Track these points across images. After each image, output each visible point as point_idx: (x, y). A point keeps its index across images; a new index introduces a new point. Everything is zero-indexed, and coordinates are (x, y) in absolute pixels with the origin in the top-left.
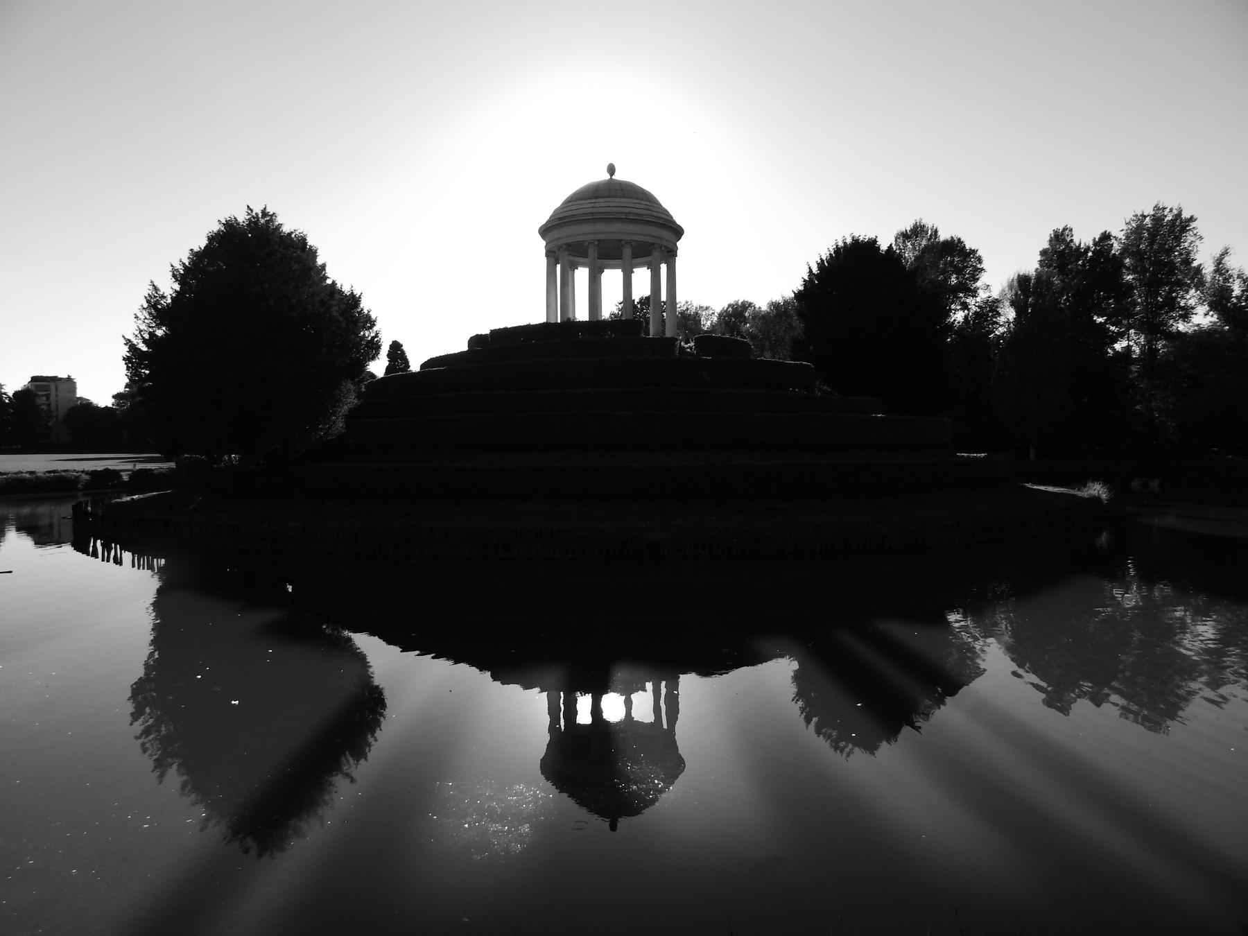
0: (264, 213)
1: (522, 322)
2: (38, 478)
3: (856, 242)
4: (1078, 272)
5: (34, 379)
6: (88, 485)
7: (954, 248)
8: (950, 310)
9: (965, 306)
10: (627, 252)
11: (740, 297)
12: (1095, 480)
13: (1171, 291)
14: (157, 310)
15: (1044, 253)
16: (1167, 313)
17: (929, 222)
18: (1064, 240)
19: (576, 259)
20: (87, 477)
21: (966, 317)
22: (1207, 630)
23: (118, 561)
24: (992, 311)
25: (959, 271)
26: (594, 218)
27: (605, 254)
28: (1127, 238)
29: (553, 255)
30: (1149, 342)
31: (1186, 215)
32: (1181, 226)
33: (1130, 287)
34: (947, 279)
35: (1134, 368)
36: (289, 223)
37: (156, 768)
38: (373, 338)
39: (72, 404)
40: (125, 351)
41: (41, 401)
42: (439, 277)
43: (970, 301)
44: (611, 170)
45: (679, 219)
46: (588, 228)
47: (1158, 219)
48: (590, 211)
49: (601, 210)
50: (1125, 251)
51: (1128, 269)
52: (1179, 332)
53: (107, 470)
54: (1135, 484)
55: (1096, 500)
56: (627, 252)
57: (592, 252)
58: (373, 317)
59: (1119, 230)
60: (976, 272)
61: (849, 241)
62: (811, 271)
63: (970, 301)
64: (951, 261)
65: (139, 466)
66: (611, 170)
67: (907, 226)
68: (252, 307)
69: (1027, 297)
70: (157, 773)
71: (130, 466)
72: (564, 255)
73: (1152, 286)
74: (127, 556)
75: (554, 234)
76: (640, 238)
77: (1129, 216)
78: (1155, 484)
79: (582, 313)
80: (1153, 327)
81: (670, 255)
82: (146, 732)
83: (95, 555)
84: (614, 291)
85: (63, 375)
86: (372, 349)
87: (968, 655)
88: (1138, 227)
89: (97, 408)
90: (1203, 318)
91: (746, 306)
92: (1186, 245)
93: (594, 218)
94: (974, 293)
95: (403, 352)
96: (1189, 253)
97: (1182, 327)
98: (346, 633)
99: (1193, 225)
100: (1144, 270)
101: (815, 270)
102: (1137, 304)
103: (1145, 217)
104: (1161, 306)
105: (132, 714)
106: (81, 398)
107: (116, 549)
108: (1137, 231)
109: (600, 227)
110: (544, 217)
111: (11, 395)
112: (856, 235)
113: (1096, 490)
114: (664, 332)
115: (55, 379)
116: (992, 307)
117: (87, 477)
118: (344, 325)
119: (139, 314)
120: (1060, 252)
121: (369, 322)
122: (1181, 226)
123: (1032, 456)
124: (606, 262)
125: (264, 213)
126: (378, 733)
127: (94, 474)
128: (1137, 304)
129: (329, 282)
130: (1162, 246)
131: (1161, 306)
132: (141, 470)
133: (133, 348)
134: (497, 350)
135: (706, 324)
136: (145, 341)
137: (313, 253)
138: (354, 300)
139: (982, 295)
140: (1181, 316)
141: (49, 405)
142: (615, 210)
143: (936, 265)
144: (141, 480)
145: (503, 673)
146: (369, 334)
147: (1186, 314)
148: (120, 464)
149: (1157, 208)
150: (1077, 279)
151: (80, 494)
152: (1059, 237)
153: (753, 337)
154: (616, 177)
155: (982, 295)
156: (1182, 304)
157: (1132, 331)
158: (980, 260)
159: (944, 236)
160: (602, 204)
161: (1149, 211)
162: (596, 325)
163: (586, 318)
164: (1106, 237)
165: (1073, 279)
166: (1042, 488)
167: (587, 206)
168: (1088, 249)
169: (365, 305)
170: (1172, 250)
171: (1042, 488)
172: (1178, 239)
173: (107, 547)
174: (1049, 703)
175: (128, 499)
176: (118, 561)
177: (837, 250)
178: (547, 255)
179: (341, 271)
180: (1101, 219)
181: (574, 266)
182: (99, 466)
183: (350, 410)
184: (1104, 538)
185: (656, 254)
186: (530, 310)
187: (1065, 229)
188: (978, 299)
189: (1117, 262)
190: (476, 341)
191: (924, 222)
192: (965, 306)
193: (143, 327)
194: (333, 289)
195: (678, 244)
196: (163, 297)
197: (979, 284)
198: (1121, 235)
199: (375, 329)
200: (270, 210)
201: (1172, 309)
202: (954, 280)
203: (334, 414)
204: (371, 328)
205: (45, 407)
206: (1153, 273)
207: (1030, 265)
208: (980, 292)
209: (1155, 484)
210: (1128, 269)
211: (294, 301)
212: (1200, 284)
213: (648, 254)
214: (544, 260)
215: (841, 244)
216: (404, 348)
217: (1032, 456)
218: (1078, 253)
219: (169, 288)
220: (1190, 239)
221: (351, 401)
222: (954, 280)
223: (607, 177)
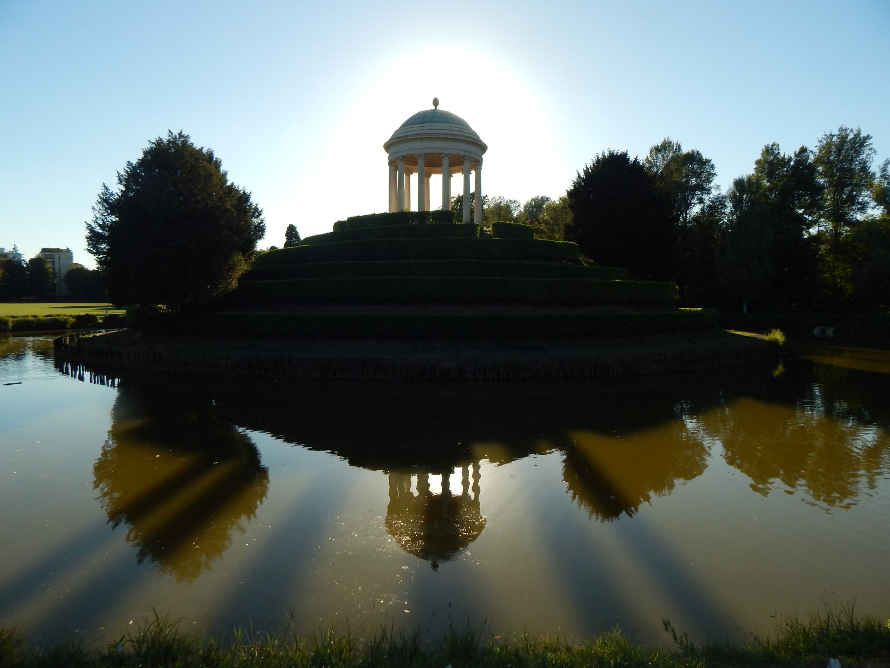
0: (180, 135)
1: (369, 212)
2: (39, 320)
3: (612, 155)
4: (784, 176)
5: (44, 250)
6: (74, 326)
7: (693, 158)
8: (691, 203)
9: (701, 201)
10: (445, 162)
11: (540, 194)
12: (776, 328)
13: (852, 191)
14: (109, 204)
15: (758, 162)
16: (849, 206)
17: (674, 140)
18: (773, 153)
19: (412, 167)
20: (74, 320)
21: (702, 210)
22: (869, 436)
23: (81, 378)
24: (721, 204)
25: (698, 175)
26: (422, 138)
27: (431, 163)
28: (820, 151)
29: (392, 163)
30: (835, 228)
31: (863, 134)
32: (859, 143)
33: (822, 188)
34: (688, 181)
35: (823, 247)
36: (199, 141)
37: (110, 520)
38: (259, 224)
39: (70, 268)
40: (87, 233)
41: (48, 265)
42: (308, 180)
43: (706, 197)
44: (436, 102)
45: (484, 139)
46: (418, 144)
47: (843, 139)
48: (418, 132)
49: (427, 132)
50: (819, 160)
51: (820, 174)
52: (857, 221)
53: (87, 315)
54: (816, 331)
55: (775, 343)
56: (445, 162)
57: (421, 161)
58: (260, 209)
59: (814, 147)
60: (711, 176)
61: (607, 154)
62: (579, 176)
63: (706, 197)
64: (690, 168)
65: (110, 312)
66: (436, 102)
67: (659, 143)
68: (175, 204)
69: (742, 194)
70: (111, 523)
71: (103, 312)
72: (401, 164)
73: (838, 186)
74: (87, 375)
75: (394, 149)
76: (455, 152)
77: (821, 136)
78: (830, 331)
79: (414, 208)
80: (838, 217)
81: (477, 164)
82: (105, 495)
83: (67, 373)
84: (437, 193)
85: (64, 248)
86: (258, 231)
87: (699, 450)
88: (828, 143)
89: (87, 271)
90: (875, 212)
91: (544, 200)
92: (864, 156)
93: (422, 138)
94: (708, 191)
95: (297, 233)
96: (865, 162)
97: (859, 217)
98: (240, 430)
99: (869, 142)
100: (833, 175)
101: (582, 174)
102: (826, 200)
103: (833, 136)
104: (845, 202)
105: (95, 482)
106: (307, 240)
107: (80, 369)
108: (827, 148)
109: (426, 144)
110: (387, 137)
111: (27, 261)
112: (612, 150)
113: (777, 336)
114: (472, 220)
115: (58, 250)
116: (719, 203)
117: (74, 320)
118: (235, 215)
119: (96, 207)
120: (770, 162)
121: (257, 212)
122: (859, 143)
123: (745, 310)
124: (433, 169)
125: (180, 135)
126: (264, 499)
127: (78, 317)
128: (826, 200)
129: (229, 184)
130: (846, 157)
131: (845, 202)
132: (111, 315)
133: (92, 230)
134: (353, 231)
135: (515, 214)
136: (99, 225)
137: (217, 164)
138: (245, 197)
139: (714, 193)
140: (859, 209)
141: (54, 269)
142: (437, 131)
143: (678, 170)
144: (110, 321)
145: (358, 459)
146: (256, 221)
147: (863, 207)
148: (97, 310)
149: (841, 130)
150: (785, 183)
151: (68, 331)
152: (769, 151)
153: (546, 222)
154: (439, 108)
155: (714, 193)
156: (860, 200)
157: (822, 220)
158: (713, 167)
159: (685, 150)
160: (428, 128)
161: (836, 132)
162: (423, 215)
163: (417, 210)
164: (803, 150)
165: (779, 181)
166: (740, 333)
167: (416, 129)
168: (790, 159)
169: (254, 200)
170: (852, 161)
171: (740, 333)
172: (858, 153)
173: (74, 369)
174: (754, 488)
175: (91, 336)
176: (81, 378)
177: (598, 161)
178: (390, 164)
179: (238, 174)
180: (801, 135)
181: (409, 173)
182: (82, 312)
183: (243, 274)
184: (779, 370)
185: (467, 163)
186: (375, 201)
187: (773, 145)
188: (711, 196)
189: (812, 169)
190: (339, 225)
191: (670, 139)
192: (701, 201)
193: (98, 216)
194: (231, 190)
195: (483, 156)
196: (112, 194)
197: (712, 185)
198: (816, 150)
199: (261, 217)
200: (185, 133)
201: (853, 203)
202: (693, 181)
203: (230, 277)
204: (258, 216)
205: (51, 270)
206: (839, 178)
207: (748, 170)
208: (713, 190)
209: (830, 331)
210: (820, 174)
211: (199, 198)
212: (869, 186)
213: (461, 163)
214: (387, 168)
215: (600, 156)
216: (298, 230)
217: (745, 310)
218: (784, 162)
219: (117, 189)
220: (867, 152)
221: (243, 267)
222: (693, 181)
223: (433, 108)
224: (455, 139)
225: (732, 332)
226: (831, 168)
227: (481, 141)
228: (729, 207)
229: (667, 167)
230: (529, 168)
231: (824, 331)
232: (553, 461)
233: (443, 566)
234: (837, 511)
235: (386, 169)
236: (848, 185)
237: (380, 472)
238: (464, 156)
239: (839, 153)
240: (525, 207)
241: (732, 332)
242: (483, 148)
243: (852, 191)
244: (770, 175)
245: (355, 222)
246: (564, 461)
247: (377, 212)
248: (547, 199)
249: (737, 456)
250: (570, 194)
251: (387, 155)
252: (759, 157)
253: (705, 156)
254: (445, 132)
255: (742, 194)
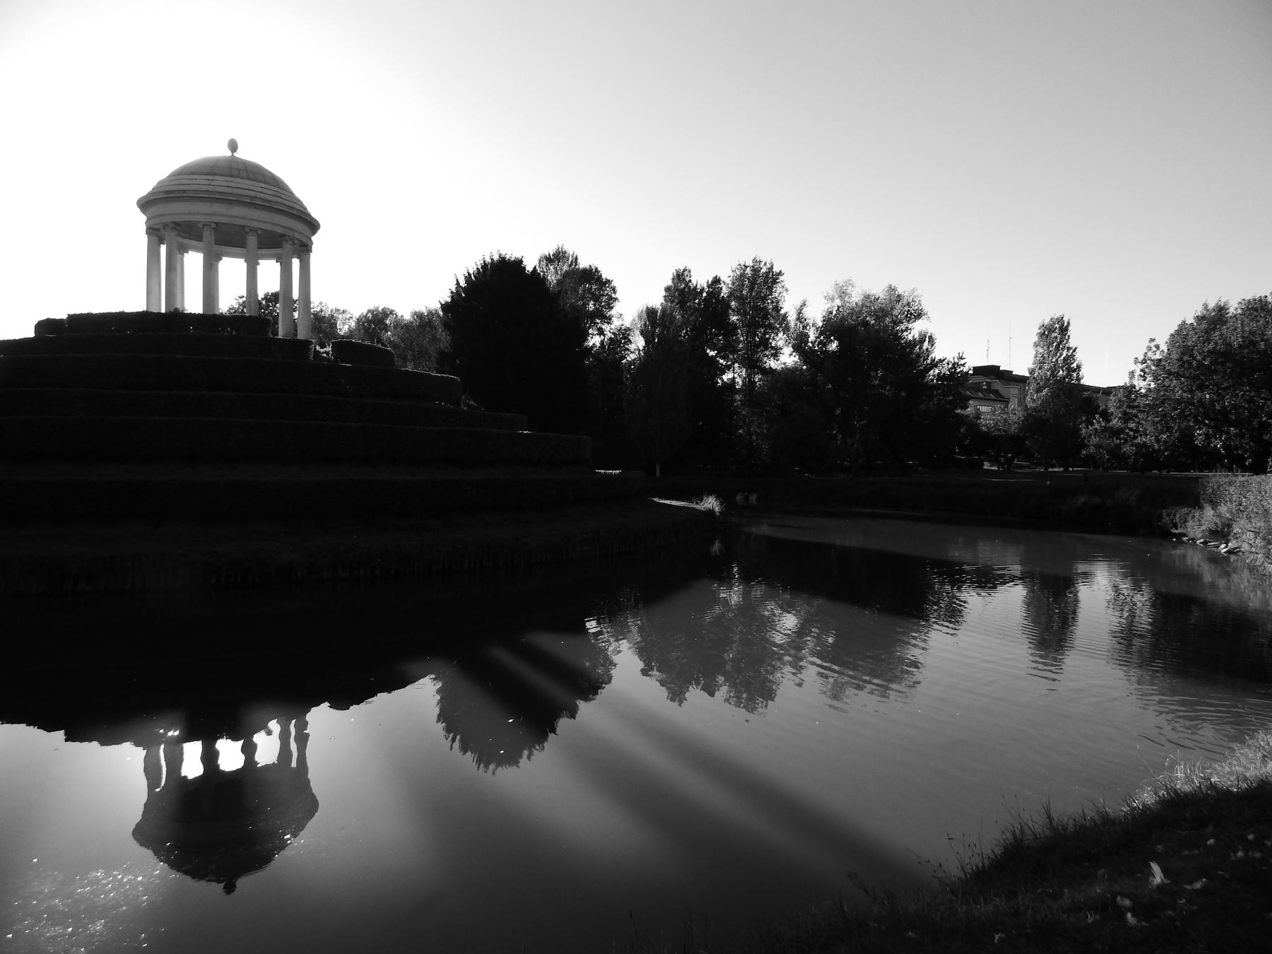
3: (503, 260)
4: (696, 310)
7: (591, 275)
9: (601, 332)
10: (252, 240)
11: (390, 306)
12: (710, 494)
13: (765, 333)
17: (570, 249)
19: (187, 241)
21: (602, 342)
22: (790, 622)
25: (597, 299)
27: (225, 240)
29: (156, 233)
30: (749, 375)
31: (776, 270)
32: (772, 279)
33: (735, 327)
34: (585, 305)
35: (738, 397)
44: (233, 146)
45: (314, 212)
46: (204, 207)
48: (204, 188)
50: (731, 294)
55: (710, 512)
59: (727, 277)
60: (611, 301)
61: (496, 258)
66: (233, 146)
67: (550, 250)
72: (170, 235)
73: (752, 326)
76: (268, 227)
77: (735, 265)
78: (753, 498)
80: (752, 364)
81: (304, 250)
91: (386, 313)
94: (608, 320)
97: (772, 364)
99: (781, 278)
100: (745, 314)
104: (758, 346)
109: (218, 208)
110: (145, 188)
112: (503, 253)
113: (711, 503)
120: (681, 290)
122: (772, 279)
123: (658, 473)
130: (759, 293)
131: (758, 346)
139: (616, 323)
142: (237, 191)
147: (776, 353)
149: (755, 261)
152: (680, 277)
154: (240, 154)
155: (616, 323)
158: (614, 290)
159: (583, 264)
160: (221, 184)
162: (210, 321)
164: (717, 281)
166: (667, 502)
170: (765, 298)
171: (667, 502)
172: (770, 289)
177: (485, 266)
185: (288, 247)
189: (725, 304)
190: (46, 326)
197: (613, 312)
198: (728, 281)
201: (766, 349)
202: (591, 306)
207: (657, 300)
209: (753, 498)
212: (786, 329)
215: (488, 260)
217: (658, 473)
218: (695, 292)
220: (779, 290)
222: (591, 306)
223: (229, 153)
224: (267, 207)
225: (656, 500)
226: (744, 304)
227: (309, 215)
228: (638, 342)
229: (559, 282)
230: (381, 265)
231: (746, 499)
232: (424, 693)
233: (243, 883)
234: (863, 702)
235: (141, 240)
236: (762, 326)
237: (127, 747)
238: (283, 235)
239: (751, 289)
240: (359, 320)
241: (656, 500)
242: (314, 226)
243: (765, 333)
244: (682, 304)
245: (80, 323)
246: (439, 691)
247: (127, 310)
248: (392, 312)
249: (651, 657)
250: (445, 307)
251: (144, 218)
252: (670, 283)
253: (605, 275)
254: (251, 193)
255: (654, 328)
